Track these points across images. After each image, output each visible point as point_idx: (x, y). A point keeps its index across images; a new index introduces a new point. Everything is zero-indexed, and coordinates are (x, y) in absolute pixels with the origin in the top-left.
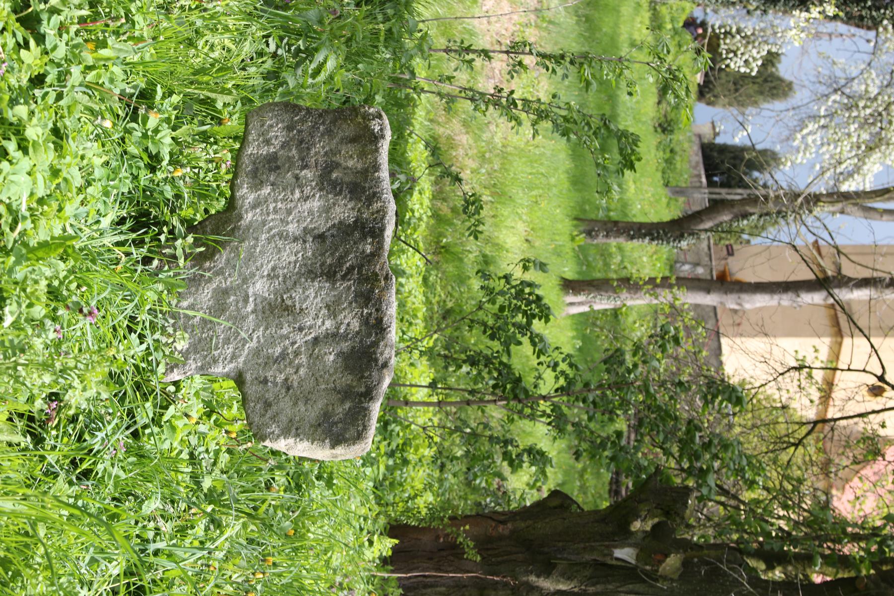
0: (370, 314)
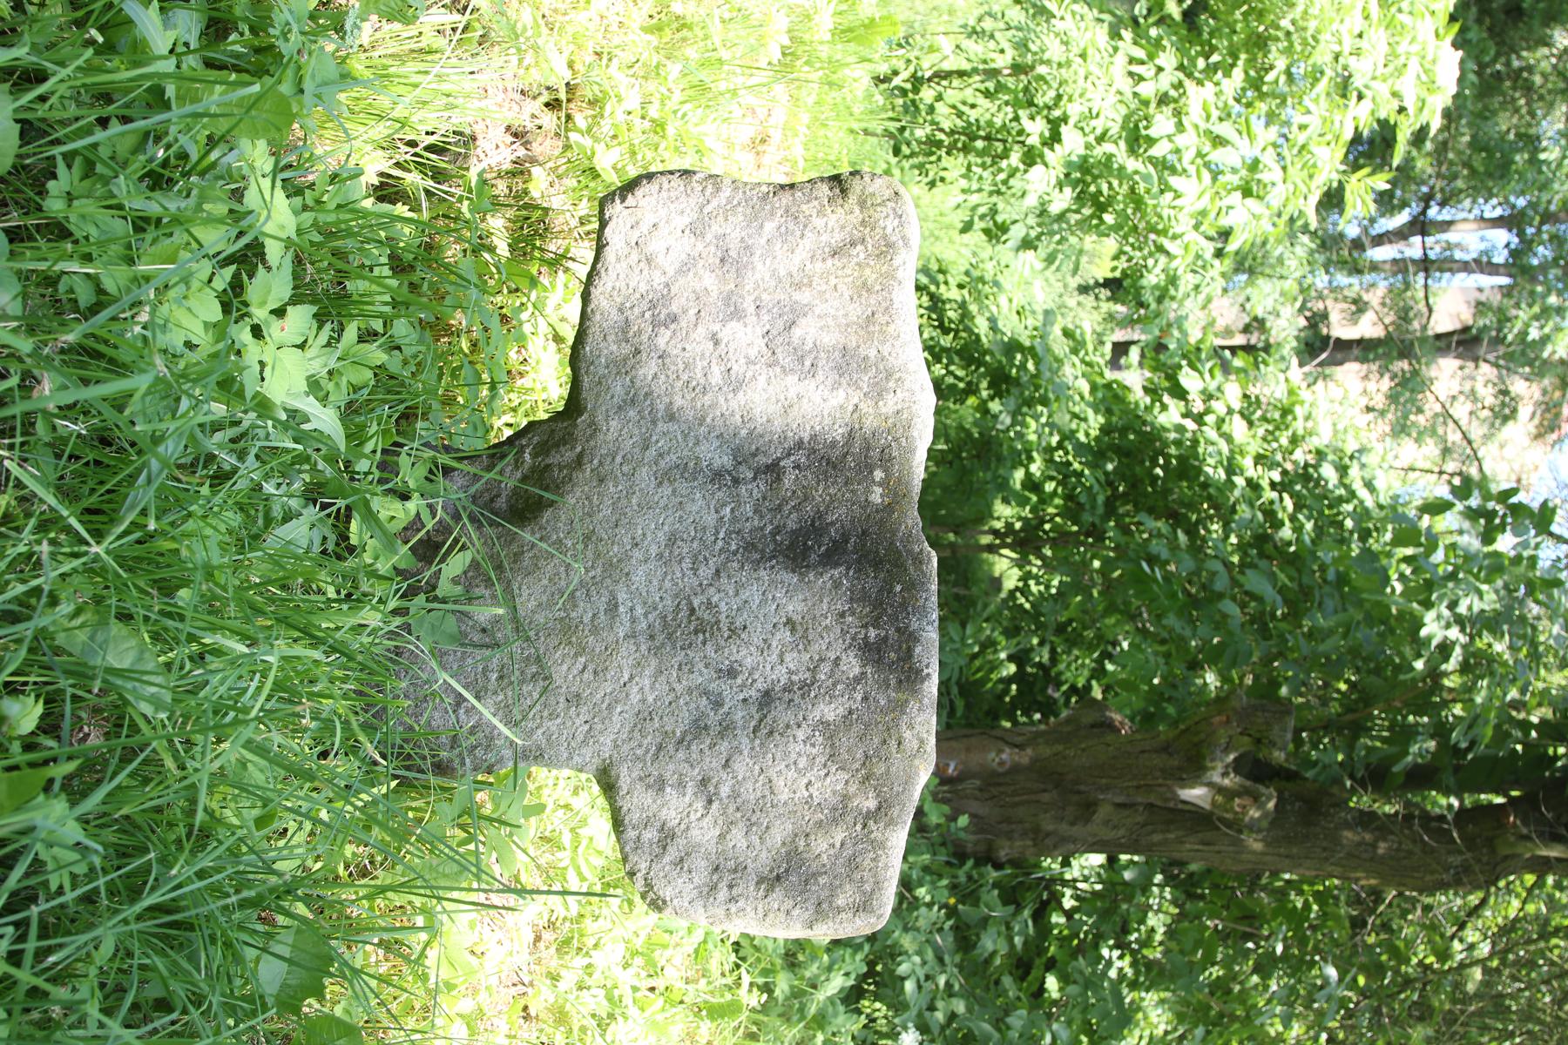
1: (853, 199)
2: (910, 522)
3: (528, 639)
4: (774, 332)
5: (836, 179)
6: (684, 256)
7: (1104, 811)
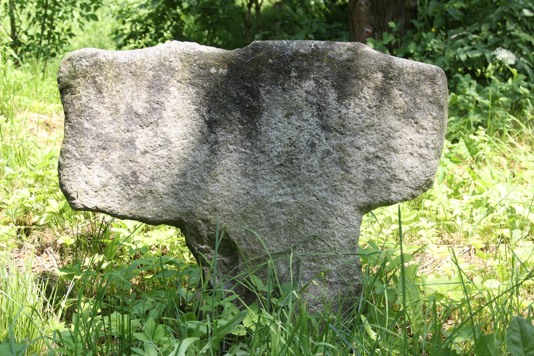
0: (297, 68)
1: (72, 82)
4: (141, 123)
6: (102, 168)
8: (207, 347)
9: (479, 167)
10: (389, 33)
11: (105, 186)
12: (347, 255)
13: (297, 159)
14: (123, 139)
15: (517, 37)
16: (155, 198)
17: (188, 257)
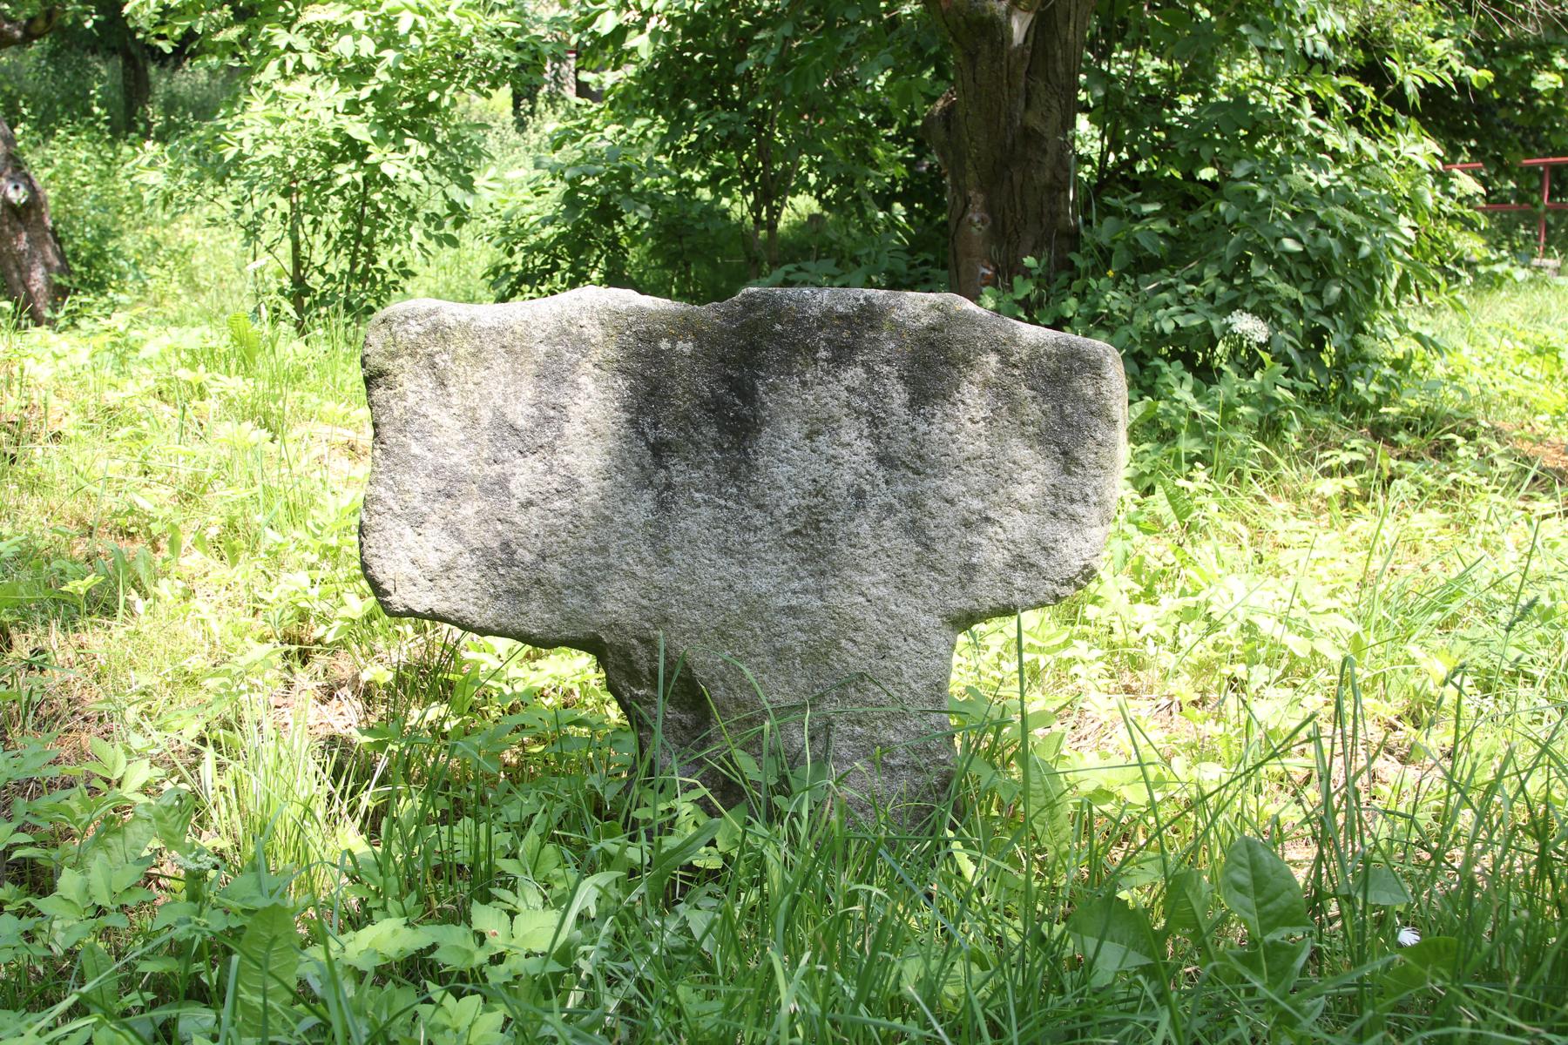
0: (829, 341)
1: (388, 365)
2: (712, 314)
3: (822, 695)
4: (520, 446)
5: (368, 381)
6: (444, 535)
7: (1033, 120)
8: (641, 889)
9: (1193, 543)
10: (1025, 278)
11: (448, 569)
12: (925, 712)
13: (829, 522)
14: (485, 477)
15: (1271, 290)
16: (546, 594)
17: (614, 713)
